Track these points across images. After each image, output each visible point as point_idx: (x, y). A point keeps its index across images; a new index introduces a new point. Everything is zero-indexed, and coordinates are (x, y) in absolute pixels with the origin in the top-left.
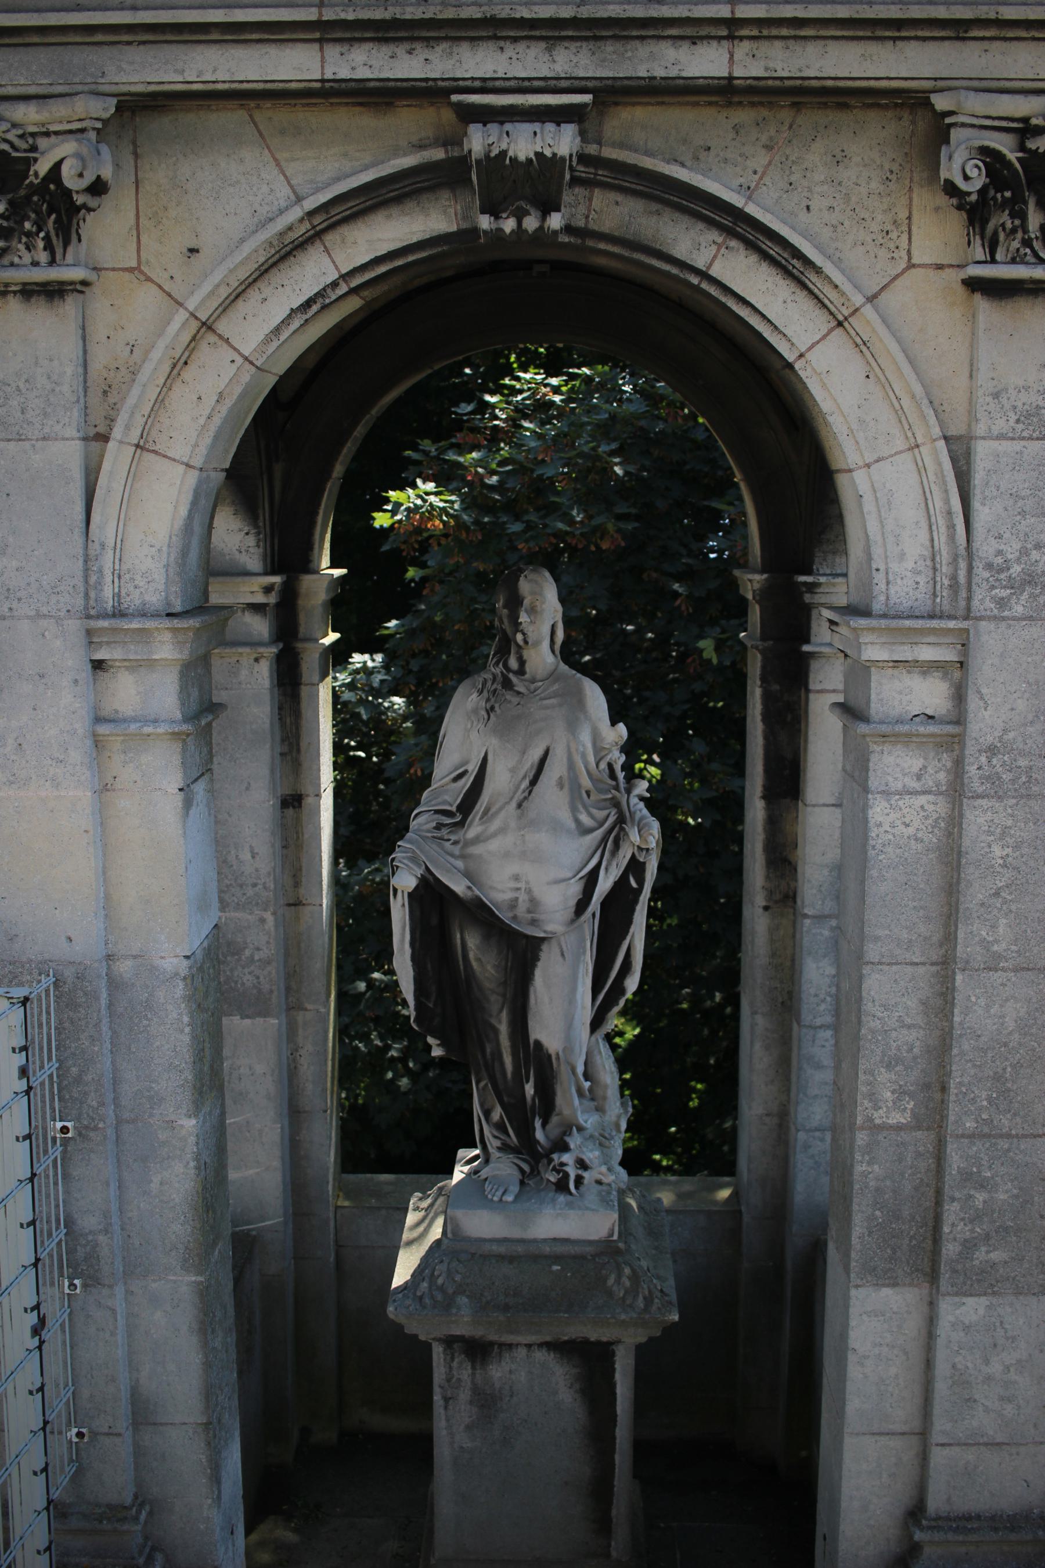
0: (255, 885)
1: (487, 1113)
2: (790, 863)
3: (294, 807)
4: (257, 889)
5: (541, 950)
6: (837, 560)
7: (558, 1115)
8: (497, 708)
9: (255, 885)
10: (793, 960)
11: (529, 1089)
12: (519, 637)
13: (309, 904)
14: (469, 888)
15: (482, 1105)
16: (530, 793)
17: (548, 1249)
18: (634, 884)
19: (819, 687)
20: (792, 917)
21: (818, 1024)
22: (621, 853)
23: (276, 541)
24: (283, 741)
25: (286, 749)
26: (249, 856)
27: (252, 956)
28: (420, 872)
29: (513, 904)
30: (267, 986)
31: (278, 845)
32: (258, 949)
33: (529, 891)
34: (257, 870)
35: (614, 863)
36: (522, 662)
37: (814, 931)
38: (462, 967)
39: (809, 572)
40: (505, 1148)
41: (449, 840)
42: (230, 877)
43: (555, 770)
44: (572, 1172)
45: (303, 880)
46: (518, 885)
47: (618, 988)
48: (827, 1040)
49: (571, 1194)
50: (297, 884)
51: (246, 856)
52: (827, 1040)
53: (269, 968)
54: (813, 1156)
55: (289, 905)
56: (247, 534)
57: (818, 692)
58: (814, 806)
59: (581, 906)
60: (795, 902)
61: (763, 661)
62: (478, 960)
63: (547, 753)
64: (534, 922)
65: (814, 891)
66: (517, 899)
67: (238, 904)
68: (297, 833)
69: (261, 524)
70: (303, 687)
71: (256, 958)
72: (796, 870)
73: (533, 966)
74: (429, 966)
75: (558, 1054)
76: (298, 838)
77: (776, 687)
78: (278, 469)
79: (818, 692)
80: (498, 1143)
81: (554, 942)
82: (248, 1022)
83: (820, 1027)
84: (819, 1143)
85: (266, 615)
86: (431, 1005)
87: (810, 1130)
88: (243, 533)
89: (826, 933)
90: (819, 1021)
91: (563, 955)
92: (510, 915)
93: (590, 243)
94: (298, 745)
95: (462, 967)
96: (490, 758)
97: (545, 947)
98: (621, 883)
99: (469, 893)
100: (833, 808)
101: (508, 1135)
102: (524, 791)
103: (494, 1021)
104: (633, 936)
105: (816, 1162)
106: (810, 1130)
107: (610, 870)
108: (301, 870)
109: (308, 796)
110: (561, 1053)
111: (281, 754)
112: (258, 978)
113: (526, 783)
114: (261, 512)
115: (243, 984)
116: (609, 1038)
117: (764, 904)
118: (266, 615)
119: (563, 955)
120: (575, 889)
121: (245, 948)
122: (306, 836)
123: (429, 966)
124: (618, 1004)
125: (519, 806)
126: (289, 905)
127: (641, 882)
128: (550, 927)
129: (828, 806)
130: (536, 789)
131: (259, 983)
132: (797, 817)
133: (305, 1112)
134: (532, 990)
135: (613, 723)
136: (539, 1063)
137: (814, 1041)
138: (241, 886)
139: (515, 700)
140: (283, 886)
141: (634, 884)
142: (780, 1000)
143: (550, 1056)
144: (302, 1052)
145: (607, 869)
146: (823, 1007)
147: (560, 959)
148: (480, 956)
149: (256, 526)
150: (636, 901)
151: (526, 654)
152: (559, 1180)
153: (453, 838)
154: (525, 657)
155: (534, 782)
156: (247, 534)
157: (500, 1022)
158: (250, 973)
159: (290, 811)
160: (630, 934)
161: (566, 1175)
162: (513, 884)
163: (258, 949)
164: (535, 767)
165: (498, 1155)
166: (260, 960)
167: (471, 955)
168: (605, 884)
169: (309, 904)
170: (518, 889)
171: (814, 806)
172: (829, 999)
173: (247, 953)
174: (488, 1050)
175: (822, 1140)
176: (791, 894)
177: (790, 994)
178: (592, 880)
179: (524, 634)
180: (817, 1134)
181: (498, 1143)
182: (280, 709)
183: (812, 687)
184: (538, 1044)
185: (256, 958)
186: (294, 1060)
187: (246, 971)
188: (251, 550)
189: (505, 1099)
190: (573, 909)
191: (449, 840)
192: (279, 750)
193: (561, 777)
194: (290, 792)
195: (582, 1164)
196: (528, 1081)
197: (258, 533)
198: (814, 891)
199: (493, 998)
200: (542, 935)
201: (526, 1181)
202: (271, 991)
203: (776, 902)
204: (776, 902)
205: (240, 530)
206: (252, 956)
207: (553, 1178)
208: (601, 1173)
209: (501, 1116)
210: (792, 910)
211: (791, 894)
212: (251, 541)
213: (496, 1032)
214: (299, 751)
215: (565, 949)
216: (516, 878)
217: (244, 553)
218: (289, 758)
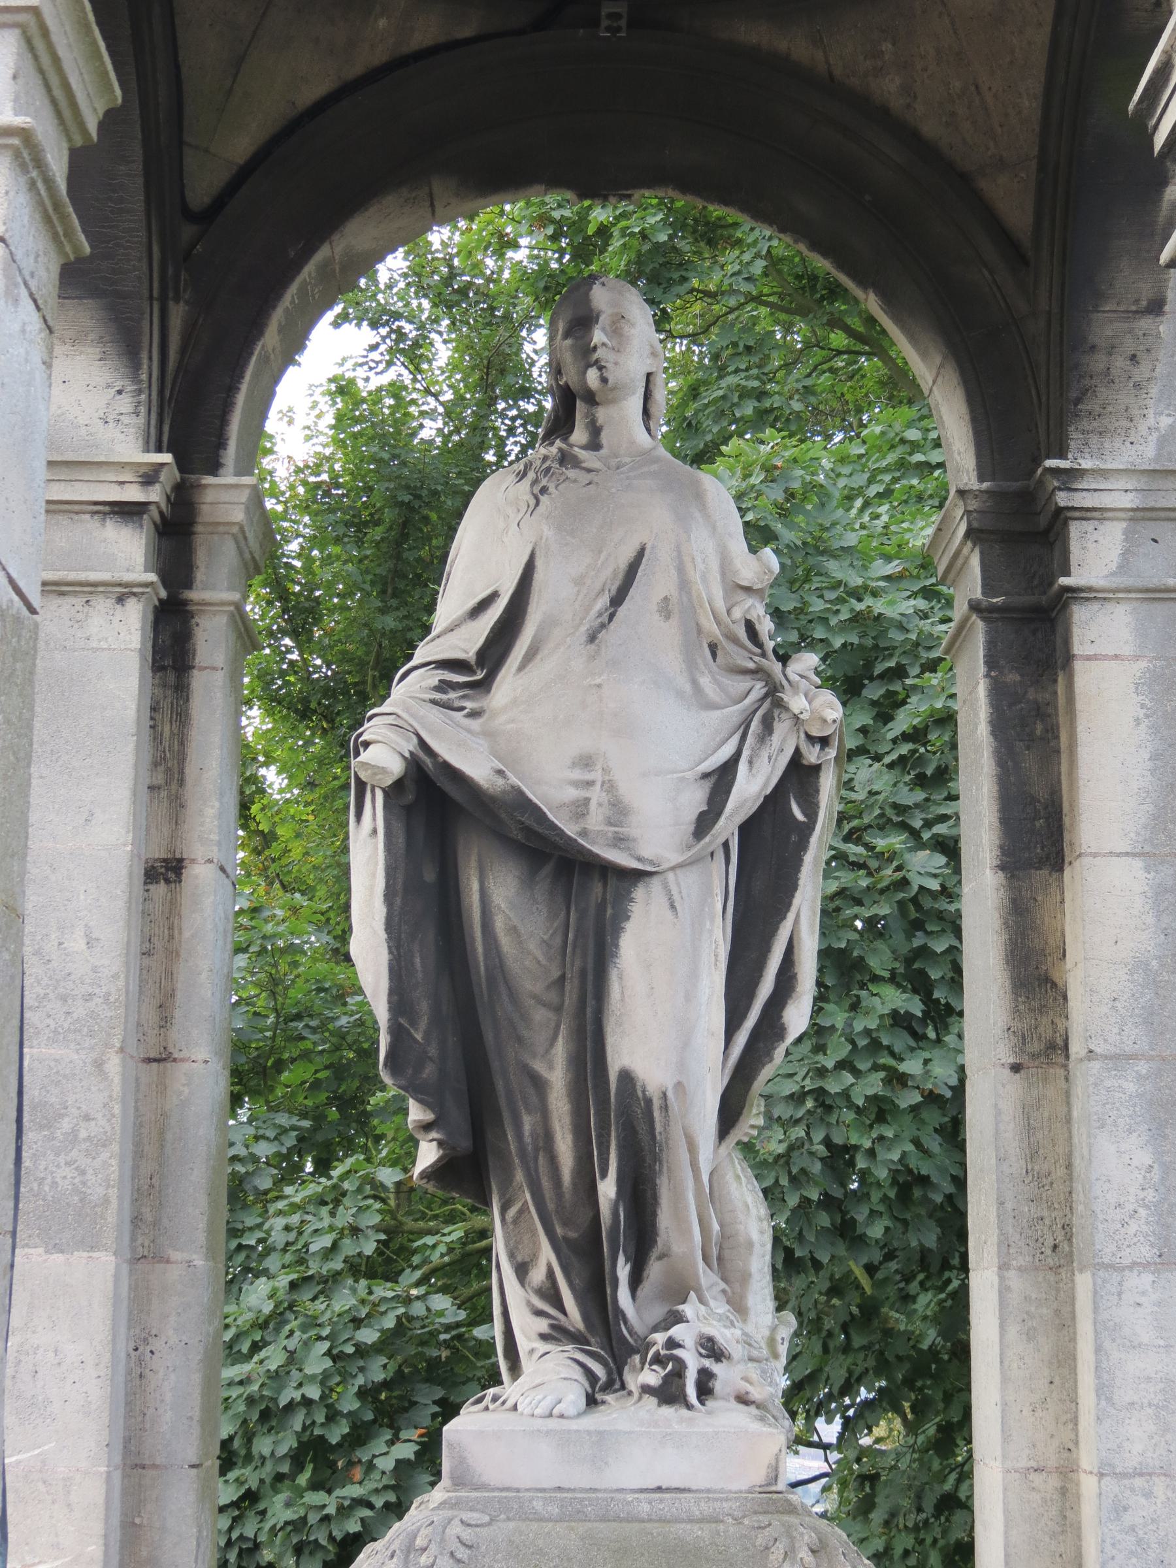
0: (89, 997)
1: (522, 1271)
2: (1054, 985)
3: (167, 881)
4: (91, 1005)
5: (632, 900)
6: (1107, 445)
7: (660, 1258)
8: (552, 489)
9: (89, 997)
10: (1069, 1166)
11: (607, 1189)
12: (592, 376)
13: (182, 1060)
14: (500, 772)
15: (512, 1256)
16: (612, 616)
17: (646, 1507)
18: (800, 816)
19: (1089, 650)
20: (1063, 1084)
21: (1127, 1261)
22: (776, 738)
23: (166, 428)
24: (155, 764)
25: (159, 779)
26: (81, 945)
27: (74, 1132)
28: (409, 746)
29: (580, 809)
30: (101, 1191)
31: (136, 949)
32: (87, 1118)
33: (610, 786)
34: (95, 970)
35: (765, 755)
36: (595, 431)
37: (1108, 1083)
38: (480, 949)
39: (1062, 455)
40: (558, 1334)
41: (462, 709)
42: (45, 981)
43: (656, 583)
44: (693, 1362)
45: (177, 1013)
46: (589, 777)
47: (771, 1026)
48: (1144, 1293)
49: (689, 1407)
50: (165, 1022)
51: (77, 943)
52: (1144, 1293)
53: (105, 1155)
54: (1133, 1529)
55: (149, 1060)
56: (120, 392)
57: (1089, 658)
58: (1095, 855)
59: (704, 823)
60: (1067, 1057)
61: (988, 633)
62: (513, 930)
63: (641, 554)
64: (619, 841)
65: (1104, 1009)
66: (587, 800)
67: (55, 1032)
68: (171, 928)
69: (144, 377)
70: (195, 672)
71: (83, 1134)
72: (1065, 998)
73: (617, 931)
74: (418, 960)
75: (664, 1096)
76: (171, 937)
77: (1013, 677)
78: (178, 314)
79: (1089, 658)
80: (543, 1325)
81: (655, 883)
82: (58, 1258)
83: (1133, 1265)
84: (1143, 1501)
85: (141, 526)
86: (419, 1037)
87: (1124, 1475)
88: (113, 391)
89: (1131, 1087)
90: (1127, 1257)
91: (673, 907)
92: (577, 828)
93: (551, 1206)
94: (182, 772)
95: (480, 949)
96: (539, 563)
97: (639, 893)
98: (774, 802)
99: (500, 782)
100: (1129, 859)
101: (563, 1311)
102: (600, 615)
103: (539, 1066)
104: (797, 921)
105: (1139, 1542)
106: (1124, 1475)
107: (756, 765)
108: (173, 996)
109: (193, 861)
110: (670, 1094)
111: (151, 788)
112: (83, 1173)
113: (604, 601)
114: (144, 355)
115: (54, 1184)
116: (747, 1148)
117: (1011, 1060)
118: (141, 526)
119: (673, 907)
120: (695, 799)
121: (61, 1116)
122: (187, 934)
123: (418, 960)
124: (771, 1060)
125: (592, 638)
126: (149, 1060)
127: (811, 810)
128: (647, 852)
129: (1118, 855)
130: (622, 611)
131: (84, 1183)
132: (1062, 902)
133: (155, 1466)
134: (613, 975)
135: (753, 550)
136: (626, 1124)
137: (1120, 1294)
138: (64, 999)
139: (584, 477)
140: (139, 1025)
141: (800, 816)
142: (1050, 1242)
143: (649, 1102)
144: (156, 1344)
145: (750, 762)
146: (1133, 1227)
147: (669, 914)
148: (516, 921)
149: (136, 380)
150: (803, 845)
151: (601, 414)
152: (667, 1379)
153: (469, 705)
154: (600, 422)
155: (617, 600)
156: (120, 392)
157: (551, 1067)
158: (67, 1164)
159: (160, 889)
160: (794, 909)
161: (681, 1365)
162: (577, 775)
163: (87, 1118)
164: (621, 576)
165: (542, 1347)
166: (89, 1139)
167: (499, 924)
168: (751, 787)
169: (182, 1060)
170: (590, 784)
171: (1095, 855)
172: (1143, 1212)
173: (66, 1125)
174: (527, 1128)
175: (1148, 1495)
176: (1060, 1042)
177: (1066, 1227)
178: (722, 779)
179: (601, 368)
180: (1138, 1482)
181: (543, 1325)
182: (154, 709)
183: (1077, 649)
184: (626, 1077)
185: (83, 1134)
186: (140, 1361)
187: (62, 1159)
188: (126, 419)
189: (559, 1231)
190: (692, 828)
191: (462, 709)
192: (148, 781)
193: (666, 599)
194: (163, 856)
195: (712, 1349)
196: (604, 1175)
197: (139, 392)
198: (1104, 1009)
199: (540, 1015)
200: (635, 865)
201: (599, 1397)
202: (106, 1201)
203: (1034, 1056)
204: (1034, 1056)
205: (108, 386)
206: (74, 1132)
207: (652, 1377)
208: (746, 1379)
209: (551, 1274)
210: (1062, 1072)
211: (1060, 1042)
212: (125, 404)
213: (539, 1085)
214: (181, 782)
215: (676, 897)
216: (586, 762)
217: (112, 425)
218: (164, 794)
